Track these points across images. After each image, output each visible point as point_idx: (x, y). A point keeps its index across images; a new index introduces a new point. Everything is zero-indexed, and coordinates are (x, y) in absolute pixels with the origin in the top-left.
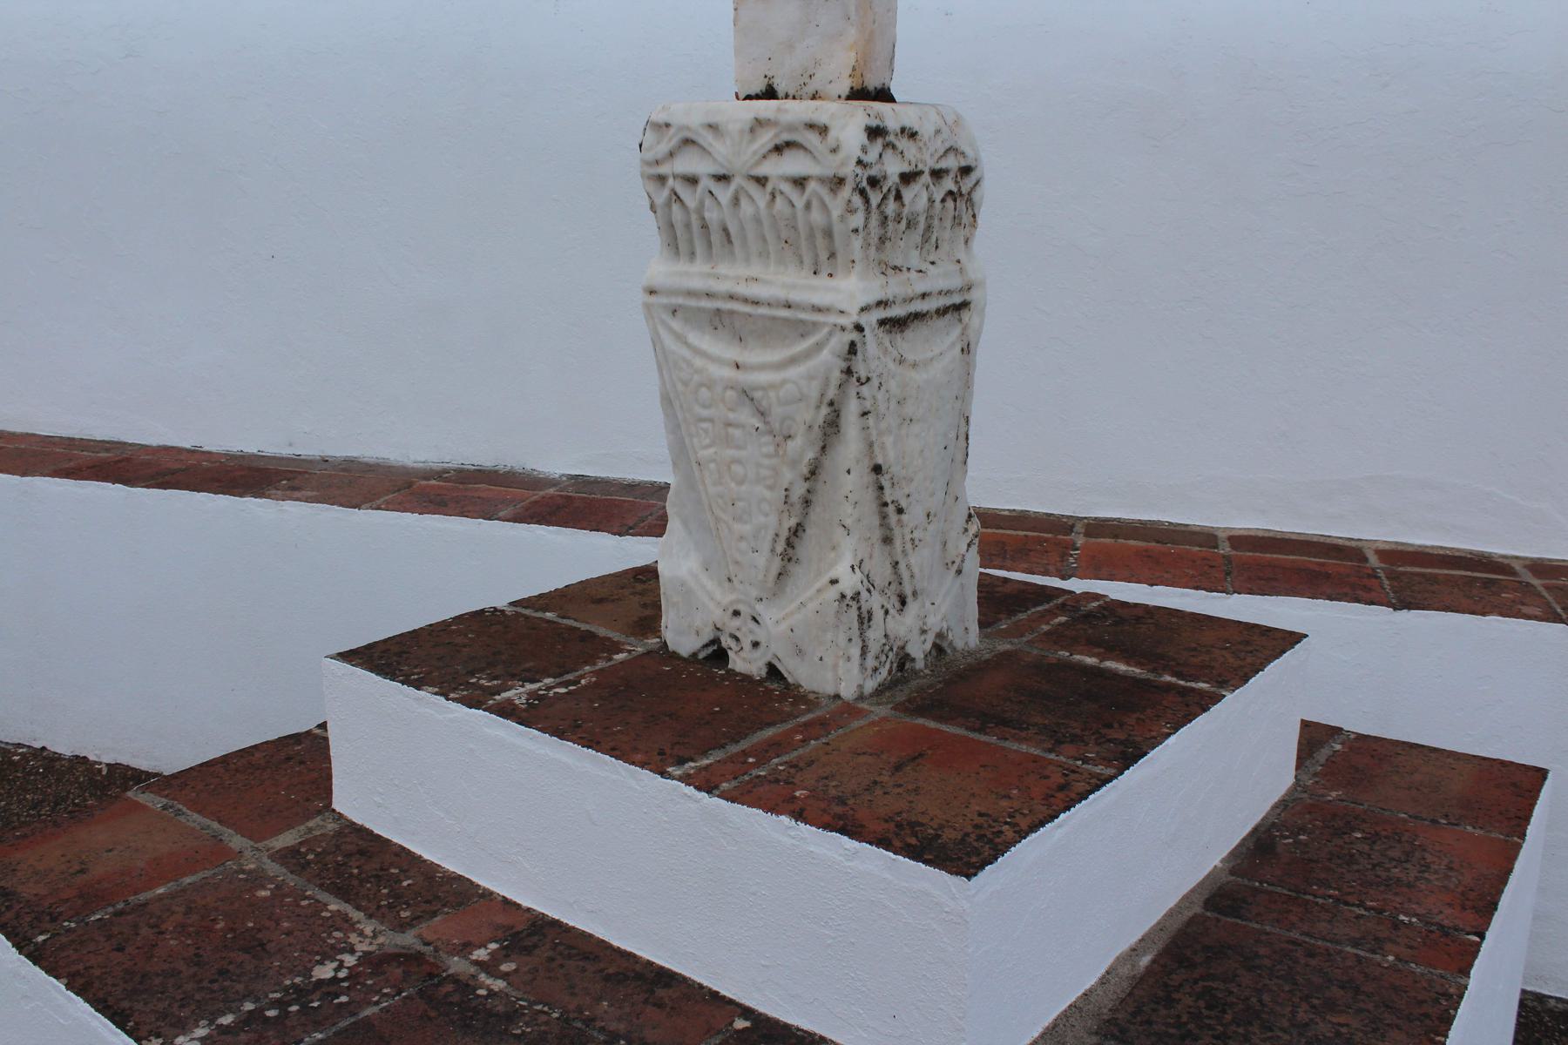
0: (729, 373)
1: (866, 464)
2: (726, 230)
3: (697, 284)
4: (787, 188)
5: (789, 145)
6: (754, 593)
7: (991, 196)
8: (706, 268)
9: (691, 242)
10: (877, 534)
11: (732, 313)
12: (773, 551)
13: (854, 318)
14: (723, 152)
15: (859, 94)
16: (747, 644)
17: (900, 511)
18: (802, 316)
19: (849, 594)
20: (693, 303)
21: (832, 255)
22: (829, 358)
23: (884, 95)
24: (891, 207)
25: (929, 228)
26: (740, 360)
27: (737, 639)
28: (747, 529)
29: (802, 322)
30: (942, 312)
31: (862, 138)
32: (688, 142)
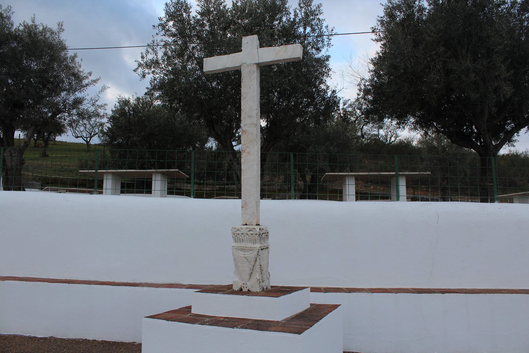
0: (243, 255)
1: (259, 265)
2: (243, 240)
3: (239, 246)
4: (250, 235)
5: (251, 230)
6: (246, 281)
7: (270, 235)
8: (240, 244)
9: (238, 241)
10: (260, 273)
11: (243, 249)
12: (249, 275)
13: (259, 248)
14: (243, 231)
15: (257, 225)
16: (245, 287)
17: (263, 270)
18: (252, 248)
19: (258, 279)
20: (238, 248)
21: (256, 242)
22: (256, 253)
23: (259, 225)
24: (261, 237)
25: (264, 239)
26: (244, 254)
27: (244, 287)
28: (245, 273)
29: (252, 249)
30: (266, 248)
31: (259, 229)
32: (238, 230)
